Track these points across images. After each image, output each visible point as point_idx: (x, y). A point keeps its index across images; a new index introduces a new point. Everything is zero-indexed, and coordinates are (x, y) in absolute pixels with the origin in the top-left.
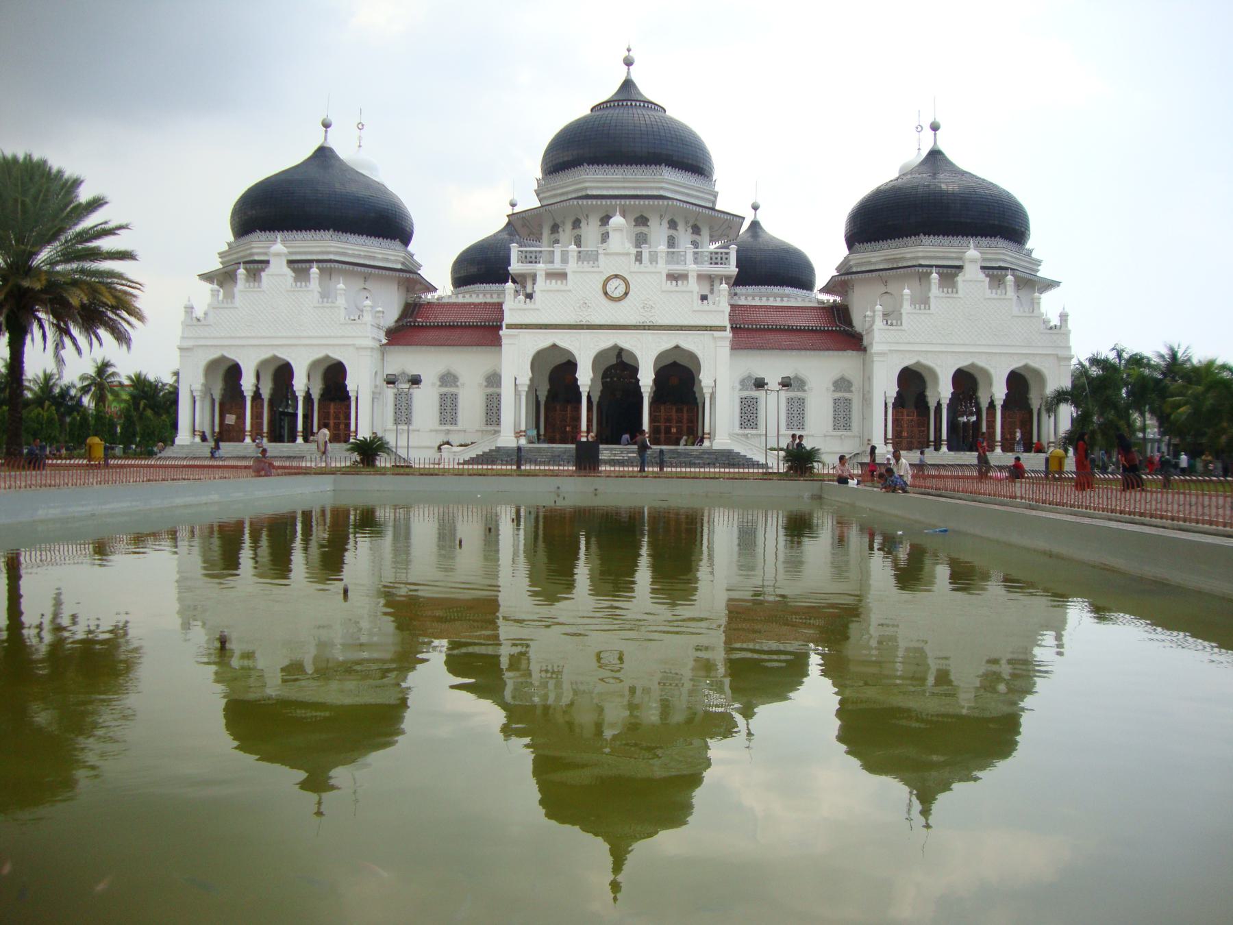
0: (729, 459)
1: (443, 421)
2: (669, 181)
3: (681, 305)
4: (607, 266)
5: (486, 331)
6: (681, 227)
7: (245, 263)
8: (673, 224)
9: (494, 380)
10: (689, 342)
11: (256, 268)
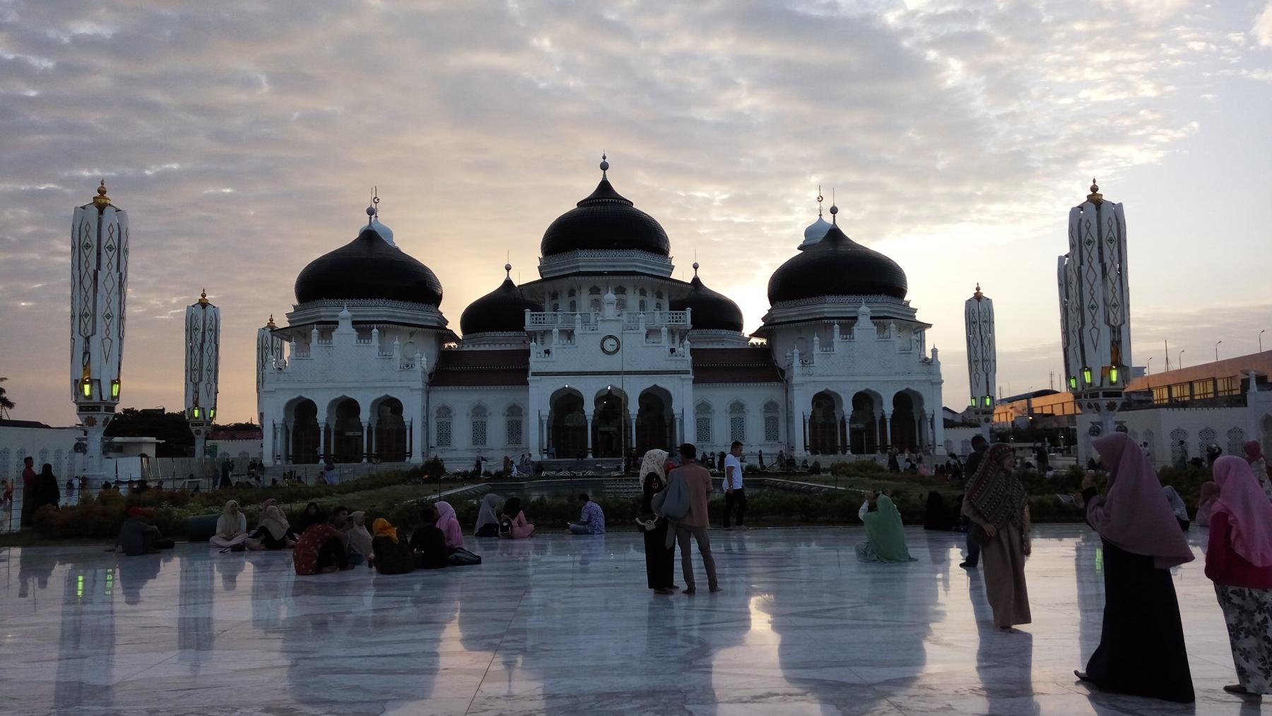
1: (475, 442)
4: (605, 330)
5: (513, 371)
6: (649, 294)
7: (318, 323)
8: (643, 292)
11: (328, 327)
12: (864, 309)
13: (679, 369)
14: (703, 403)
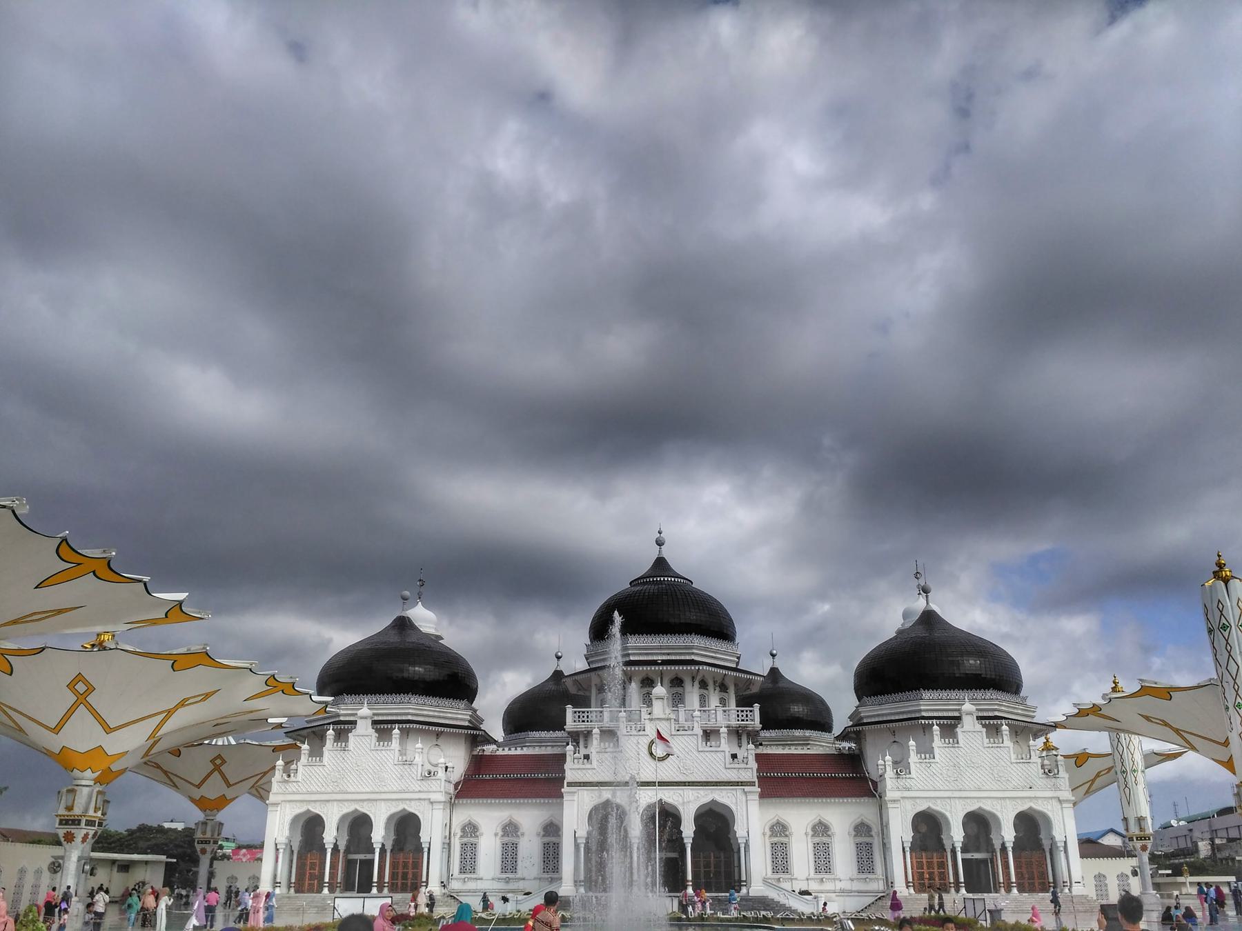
0: (764, 903)
1: (504, 869)
2: (700, 647)
3: (715, 761)
5: (544, 781)
6: (711, 687)
7: (334, 723)
8: (703, 685)
9: (552, 830)
10: (724, 797)
11: (344, 729)
12: (968, 707)
13: (585, 780)
14: (778, 823)
